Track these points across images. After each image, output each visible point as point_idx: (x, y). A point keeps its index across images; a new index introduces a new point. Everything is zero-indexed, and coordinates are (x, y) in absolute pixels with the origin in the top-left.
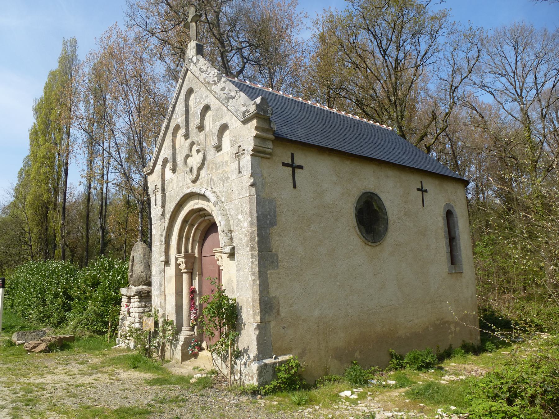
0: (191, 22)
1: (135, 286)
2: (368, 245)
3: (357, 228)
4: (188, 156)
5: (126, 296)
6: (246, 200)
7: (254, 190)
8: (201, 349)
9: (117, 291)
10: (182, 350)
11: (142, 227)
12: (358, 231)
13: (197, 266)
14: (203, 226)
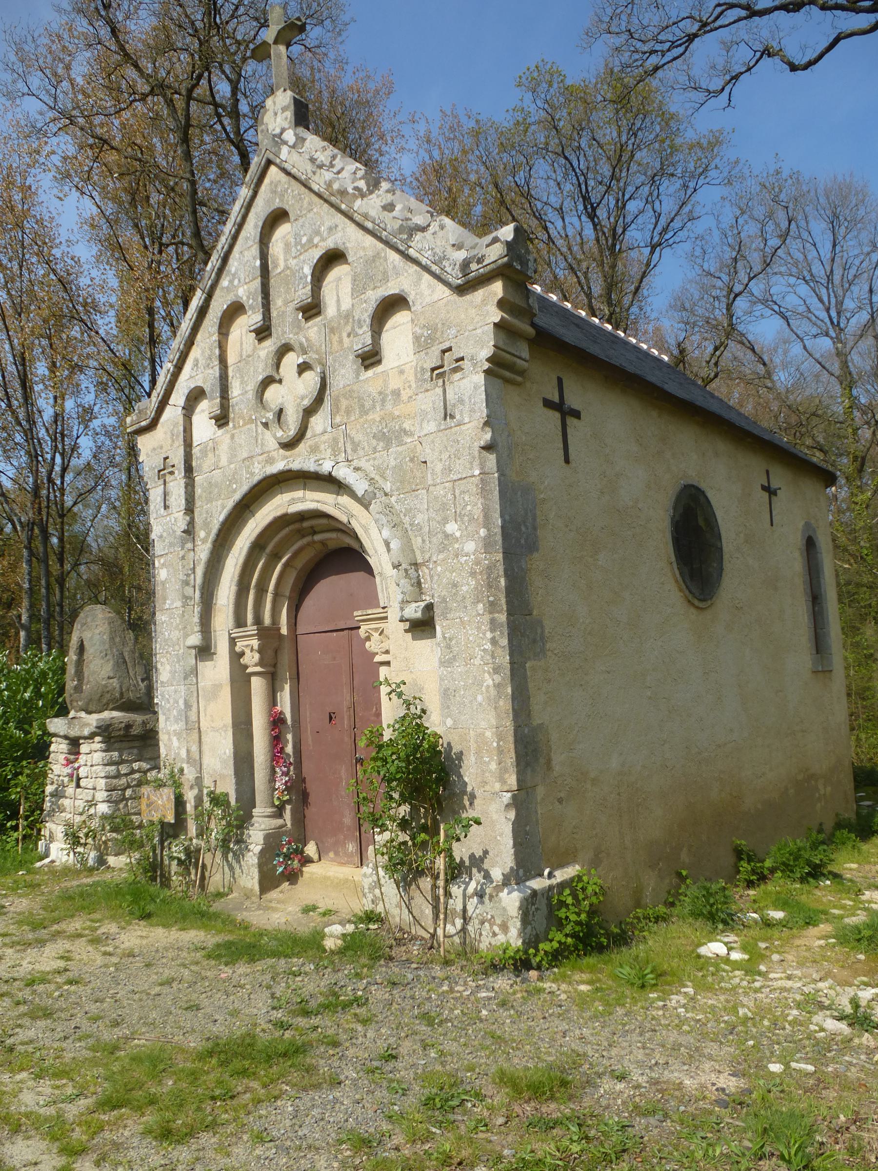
0: (276, 42)
1: (89, 713)
2: (693, 605)
3: (675, 565)
4: (268, 381)
5: (66, 737)
6: (472, 485)
7: (492, 459)
8: (308, 861)
9: (26, 727)
10: (261, 866)
11: (30, 582)
12: (677, 572)
13: (286, 658)
14: (323, 555)
